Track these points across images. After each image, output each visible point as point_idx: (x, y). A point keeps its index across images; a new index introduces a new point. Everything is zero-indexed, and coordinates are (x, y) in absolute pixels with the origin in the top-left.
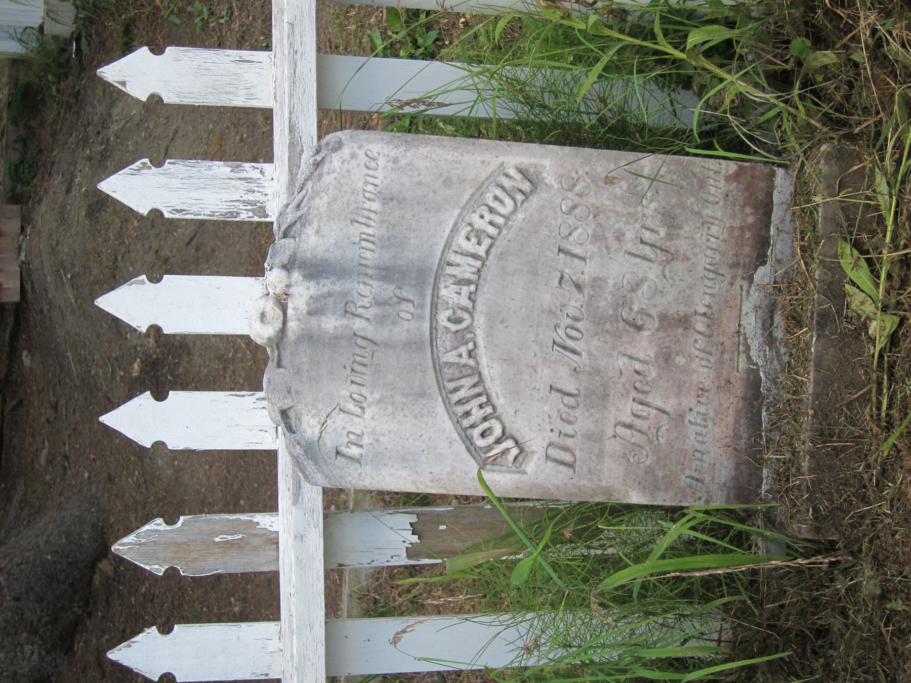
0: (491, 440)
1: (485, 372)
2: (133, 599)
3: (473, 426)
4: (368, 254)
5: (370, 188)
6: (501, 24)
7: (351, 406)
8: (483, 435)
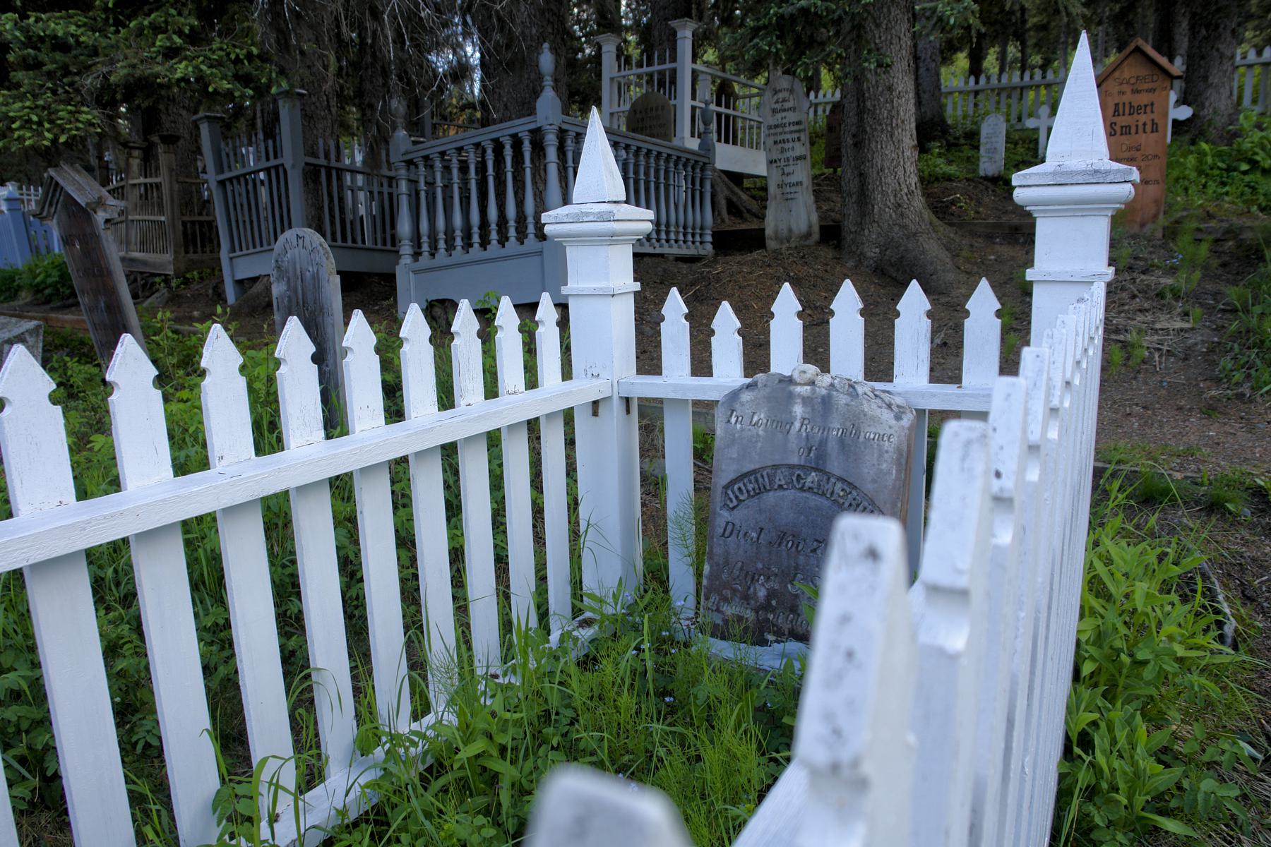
0: (738, 494)
1: (771, 494)
2: (992, 257)
3: (744, 485)
4: (835, 433)
5: (872, 436)
6: (92, 212)
7: (755, 419)
8: (740, 489)
